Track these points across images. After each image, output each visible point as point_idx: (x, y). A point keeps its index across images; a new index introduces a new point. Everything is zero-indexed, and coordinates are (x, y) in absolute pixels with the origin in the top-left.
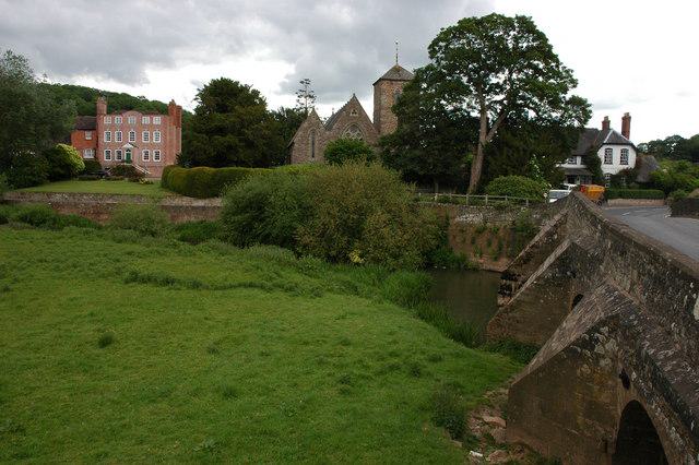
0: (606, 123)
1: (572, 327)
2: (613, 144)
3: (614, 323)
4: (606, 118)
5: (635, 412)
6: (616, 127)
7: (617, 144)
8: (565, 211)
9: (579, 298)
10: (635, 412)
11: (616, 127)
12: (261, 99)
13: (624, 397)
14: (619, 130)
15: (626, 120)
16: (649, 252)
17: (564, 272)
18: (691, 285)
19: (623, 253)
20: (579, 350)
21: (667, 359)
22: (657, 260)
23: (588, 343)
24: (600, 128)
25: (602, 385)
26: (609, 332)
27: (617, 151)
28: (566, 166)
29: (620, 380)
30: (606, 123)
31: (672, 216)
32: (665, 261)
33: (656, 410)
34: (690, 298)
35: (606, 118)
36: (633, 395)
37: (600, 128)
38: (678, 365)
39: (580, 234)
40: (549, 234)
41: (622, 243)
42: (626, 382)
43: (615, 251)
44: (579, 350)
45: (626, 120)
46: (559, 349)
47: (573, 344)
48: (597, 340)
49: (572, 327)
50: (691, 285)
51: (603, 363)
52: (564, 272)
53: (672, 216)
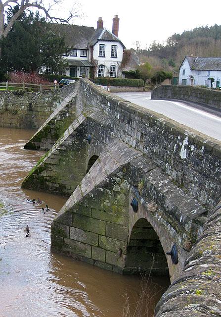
0: (100, 23)
1: (96, 176)
2: (106, 41)
3: (128, 171)
4: (100, 18)
5: (144, 226)
6: (108, 26)
7: (108, 41)
8: (73, 95)
9: (94, 159)
10: (144, 226)
11: (108, 26)
12: (159, 46)
13: (134, 217)
14: (110, 30)
15: (116, 21)
16: (149, 119)
17: (81, 141)
18: (179, 138)
19: (130, 121)
20: (102, 190)
21: (164, 185)
22: (155, 124)
23: (108, 185)
24: (95, 27)
25: (119, 213)
26: (124, 176)
27: (108, 46)
28: (69, 58)
29: (131, 207)
30: (100, 23)
31: (152, 98)
32: (161, 123)
33: (158, 222)
34: (178, 145)
35: (100, 18)
36: (140, 214)
37: (95, 27)
38: (171, 188)
39: (95, 111)
40: (62, 113)
41: (129, 114)
42: (136, 209)
43: (123, 121)
44: (102, 190)
45: (116, 21)
46: (88, 191)
47: (98, 186)
48: (115, 182)
49: (96, 176)
50: (179, 138)
51: (119, 197)
52: (81, 141)
53: (152, 98)
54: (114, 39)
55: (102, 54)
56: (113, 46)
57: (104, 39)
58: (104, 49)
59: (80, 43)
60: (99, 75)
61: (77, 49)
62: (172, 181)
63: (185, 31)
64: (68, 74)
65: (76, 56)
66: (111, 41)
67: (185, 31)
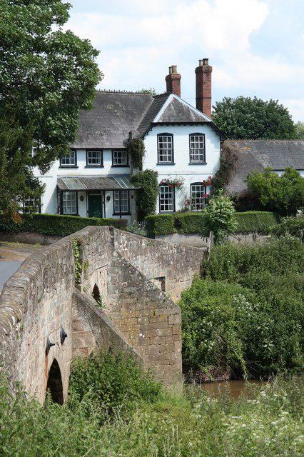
2: (173, 124)
4: (172, 68)
7: (179, 124)
15: (203, 73)
30: (173, 82)
35: (172, 68)
45: (203, 73)
54: (194, 119)
55: (166, 155)
56: (193, 137)
57: (167, 121)
58: (171, 146)
59: (109, 133)
60: (162, 208)
61: (102, 150)
62: (226, 414)
63: (96, 53)
64: (83, 213)
65: (76, 167)
66: (185, 124)
67: (96, 53)
